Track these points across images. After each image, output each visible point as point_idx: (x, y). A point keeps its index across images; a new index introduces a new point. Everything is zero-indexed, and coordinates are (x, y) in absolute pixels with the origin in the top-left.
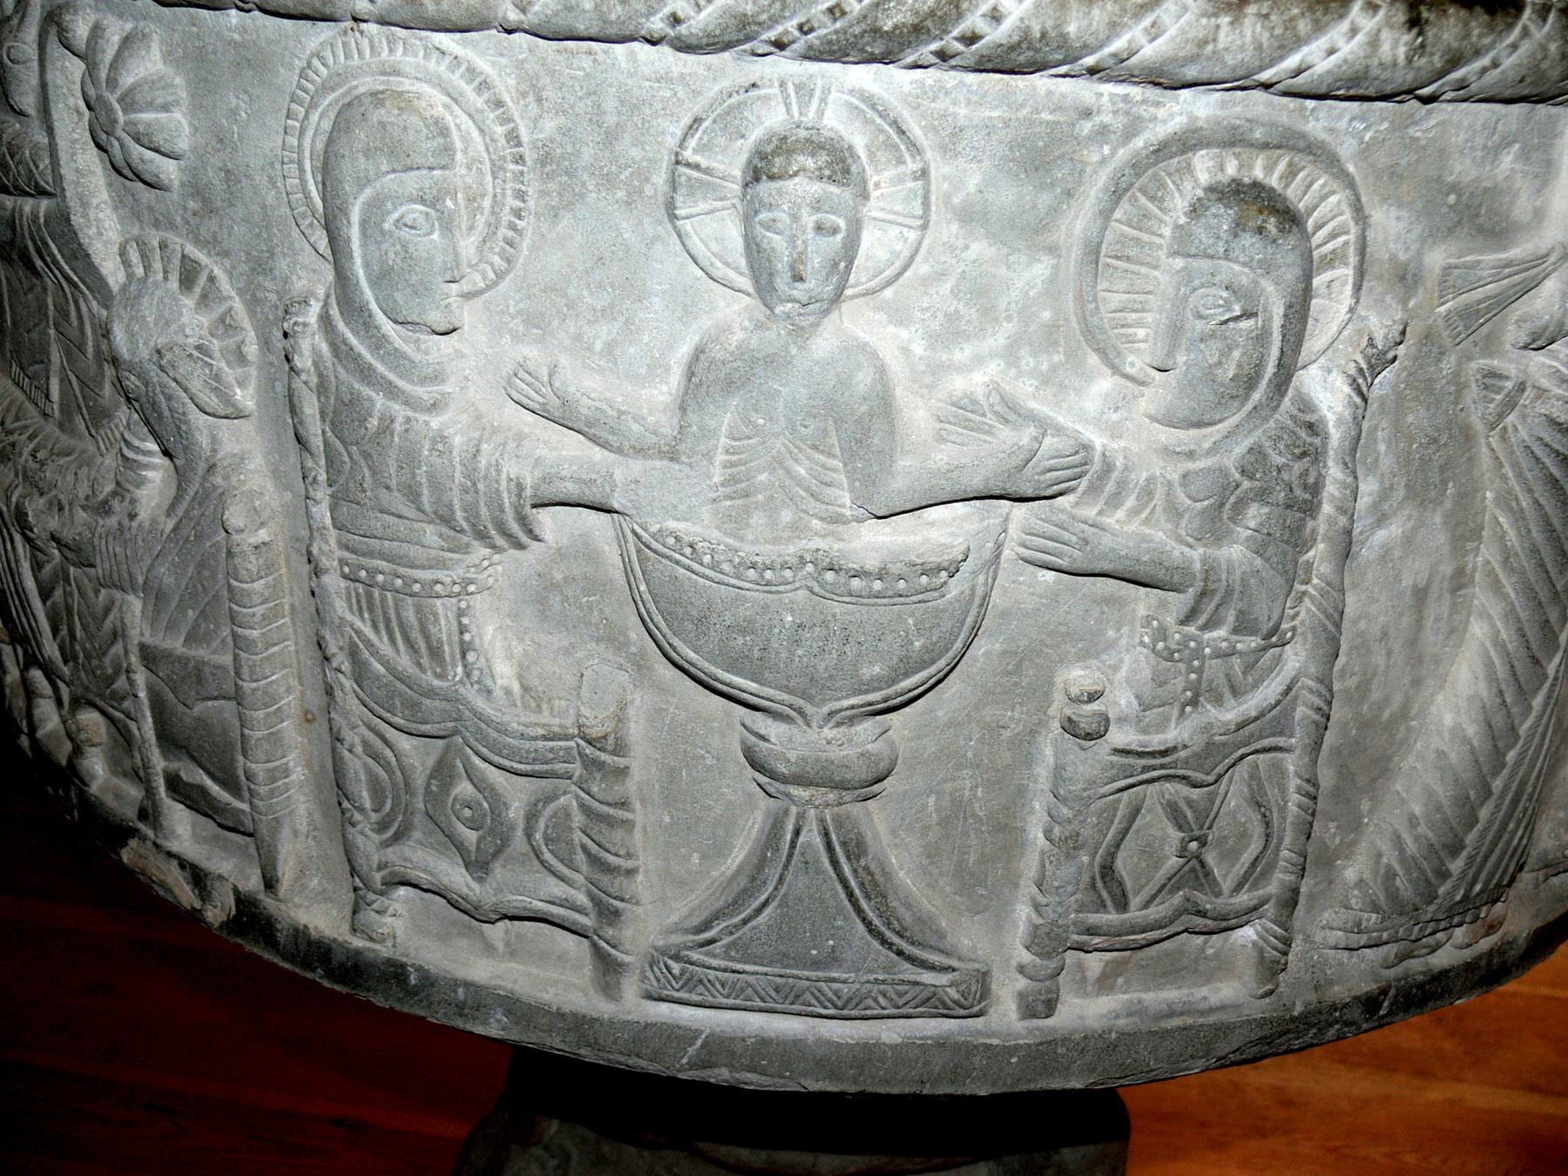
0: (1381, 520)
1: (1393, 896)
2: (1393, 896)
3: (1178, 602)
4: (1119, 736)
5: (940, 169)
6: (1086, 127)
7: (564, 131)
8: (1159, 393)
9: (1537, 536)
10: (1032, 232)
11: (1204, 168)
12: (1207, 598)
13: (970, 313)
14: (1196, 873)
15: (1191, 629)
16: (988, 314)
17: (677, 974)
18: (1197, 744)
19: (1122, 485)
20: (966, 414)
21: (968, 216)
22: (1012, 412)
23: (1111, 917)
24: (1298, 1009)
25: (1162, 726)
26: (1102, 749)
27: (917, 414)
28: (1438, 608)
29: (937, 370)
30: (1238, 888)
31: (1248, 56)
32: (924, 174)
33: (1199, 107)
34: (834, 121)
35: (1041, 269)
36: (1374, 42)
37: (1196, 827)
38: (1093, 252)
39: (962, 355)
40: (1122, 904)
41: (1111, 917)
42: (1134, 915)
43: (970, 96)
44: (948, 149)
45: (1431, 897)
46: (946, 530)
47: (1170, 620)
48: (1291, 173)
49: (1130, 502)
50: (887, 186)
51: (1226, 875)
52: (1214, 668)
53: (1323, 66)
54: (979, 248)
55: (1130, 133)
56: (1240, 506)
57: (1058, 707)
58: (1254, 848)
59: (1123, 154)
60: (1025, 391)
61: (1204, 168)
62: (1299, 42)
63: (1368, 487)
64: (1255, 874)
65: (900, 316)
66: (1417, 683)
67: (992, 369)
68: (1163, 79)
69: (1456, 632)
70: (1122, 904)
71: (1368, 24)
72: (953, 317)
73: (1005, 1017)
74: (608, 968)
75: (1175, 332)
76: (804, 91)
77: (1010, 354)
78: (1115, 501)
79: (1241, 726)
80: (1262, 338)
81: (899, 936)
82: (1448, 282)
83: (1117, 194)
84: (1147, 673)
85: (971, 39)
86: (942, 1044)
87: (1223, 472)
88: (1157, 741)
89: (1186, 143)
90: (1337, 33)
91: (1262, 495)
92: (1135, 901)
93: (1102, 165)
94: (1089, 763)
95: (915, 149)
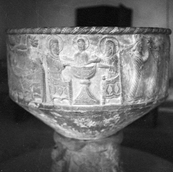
0: (124, 64)
1: (131, 96)
2: (131, 96)
3: (109, 69)
4: (106, 80)
5: (90, 41)
6: (99, 37)
7: (65, 40)
8: (106, 55)
9: (136, 65)
10: (96, 44)
11: (107, 40)
12: (111, 68)
13: (92, 50)
14: (113, 91)
15: (110, 71)
16: (94, 50)
17: (77, 102)
18: (112, 80)
19: (104, 61)
20: (93, 57)
21: (92, 44)
22: (95, 56)
23: (107, 95)
24: (125, 106)
25: (109, 79)
26: (105, 80)
27: (90, 57)
28: (130, 71)
29: (90, 54)
30: (117, 93)
31: (108, 32)
32: (88, 41)
33: (106, 36)
34: (83, 38)
35: (97, 47)
36: (116, 30)
37: (113, 88)
38: (100, 46)
39: (92, 53)
40: (108, 94)
41: (107, 95)
42: (109, 95)
43: (91, 36)
44: (90, 39)
45: (135, 96)
46: (92, 65)
47: (109, 71)
48: (113, 39)
49: (104, 62)
50: (87, 42)
51: (116, 92)
52: (112, 75)
53: (113, 32)
54: (93, 46)
55: (102, 38)
56: (112, 62)
57: (102, 78)
58: (118, 90)
59: (101, 39)
60: (96, 55)
61: (107, 40)
62: (111, 31)
63: (123, 62)
64: (119, 92)
65: (88, 51)
66: (130, 78)
67: (94, 54)
68: (103, 34)
69: (133, 73)
70: (108, 94)
71: (116, 29)
72: (91, 50)
73: (101, 105)
74: (71, 103)
75: (106, 50)
76: (81, 36)
77: (95, 53)
78: (103, 62)
79: (115, 79)
80: (112, 50)
81: (92, 97)
82: (126, 47)
83: (101, 42)
84: (108, 75)
85: (90, 32)
86: (96, 107)
87: (110, 60)
88: (109, 80)
89: (105, 38)
90: (114, 30)
91: (113, 61)
92: (110, 94)
93: (100, 40)
94: (104, 82)
95: (88, 39)
